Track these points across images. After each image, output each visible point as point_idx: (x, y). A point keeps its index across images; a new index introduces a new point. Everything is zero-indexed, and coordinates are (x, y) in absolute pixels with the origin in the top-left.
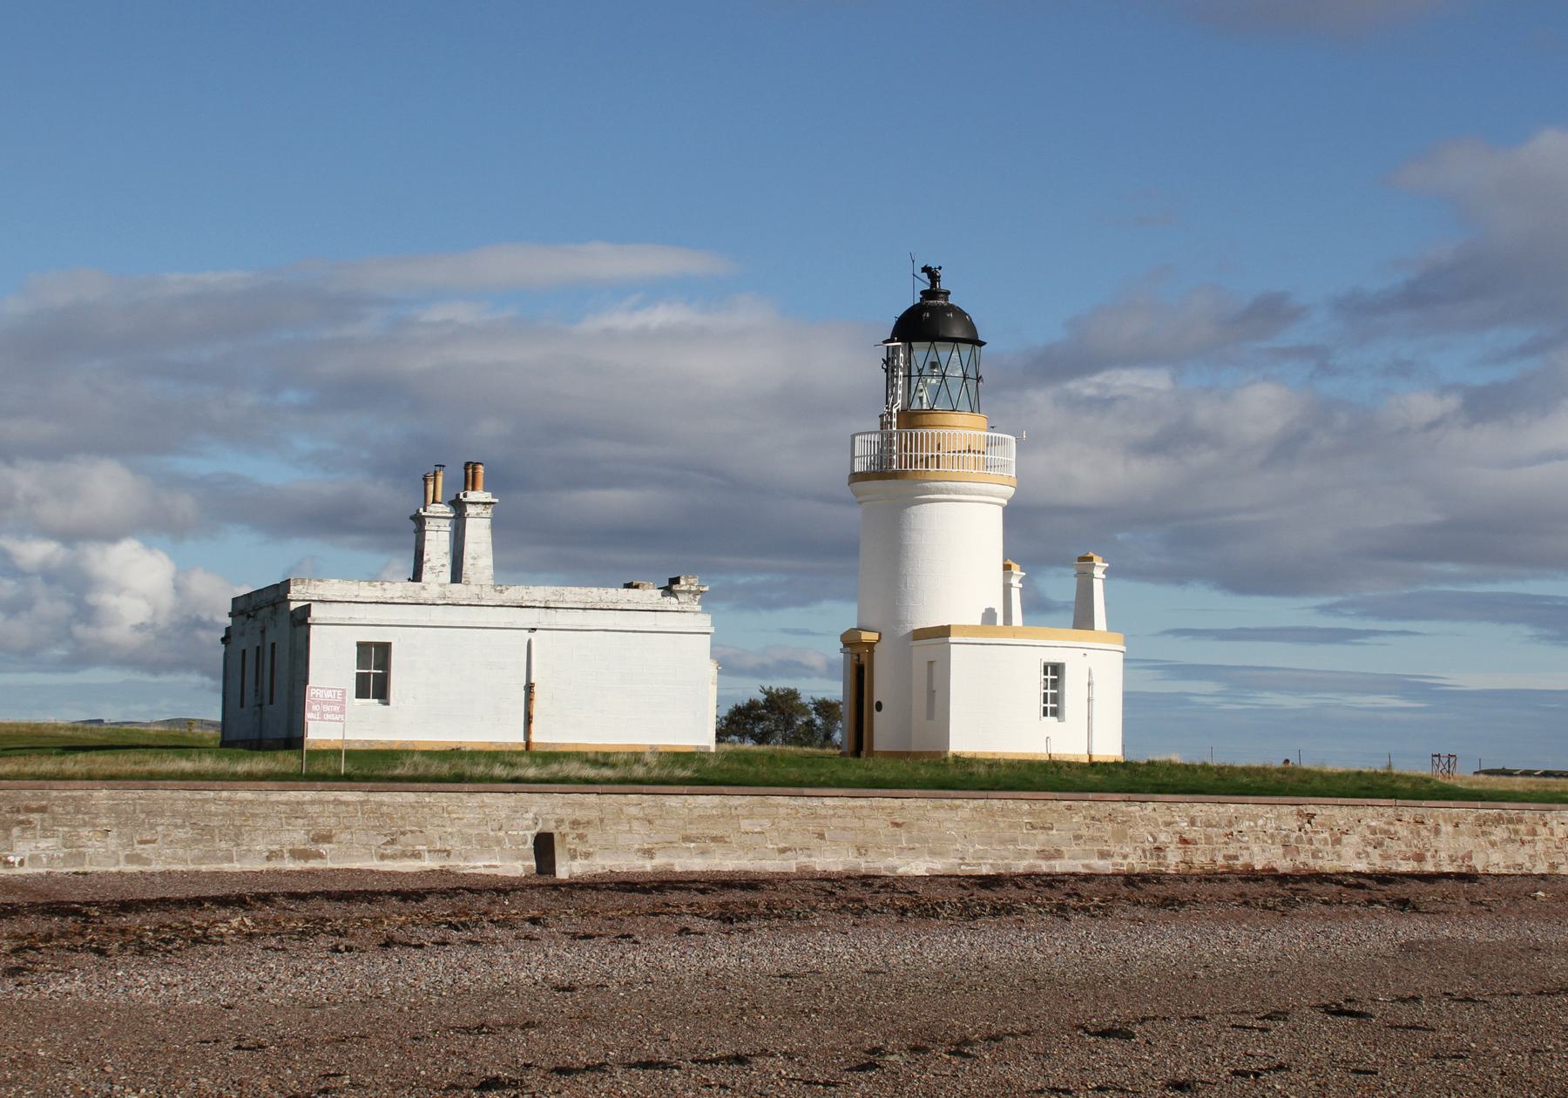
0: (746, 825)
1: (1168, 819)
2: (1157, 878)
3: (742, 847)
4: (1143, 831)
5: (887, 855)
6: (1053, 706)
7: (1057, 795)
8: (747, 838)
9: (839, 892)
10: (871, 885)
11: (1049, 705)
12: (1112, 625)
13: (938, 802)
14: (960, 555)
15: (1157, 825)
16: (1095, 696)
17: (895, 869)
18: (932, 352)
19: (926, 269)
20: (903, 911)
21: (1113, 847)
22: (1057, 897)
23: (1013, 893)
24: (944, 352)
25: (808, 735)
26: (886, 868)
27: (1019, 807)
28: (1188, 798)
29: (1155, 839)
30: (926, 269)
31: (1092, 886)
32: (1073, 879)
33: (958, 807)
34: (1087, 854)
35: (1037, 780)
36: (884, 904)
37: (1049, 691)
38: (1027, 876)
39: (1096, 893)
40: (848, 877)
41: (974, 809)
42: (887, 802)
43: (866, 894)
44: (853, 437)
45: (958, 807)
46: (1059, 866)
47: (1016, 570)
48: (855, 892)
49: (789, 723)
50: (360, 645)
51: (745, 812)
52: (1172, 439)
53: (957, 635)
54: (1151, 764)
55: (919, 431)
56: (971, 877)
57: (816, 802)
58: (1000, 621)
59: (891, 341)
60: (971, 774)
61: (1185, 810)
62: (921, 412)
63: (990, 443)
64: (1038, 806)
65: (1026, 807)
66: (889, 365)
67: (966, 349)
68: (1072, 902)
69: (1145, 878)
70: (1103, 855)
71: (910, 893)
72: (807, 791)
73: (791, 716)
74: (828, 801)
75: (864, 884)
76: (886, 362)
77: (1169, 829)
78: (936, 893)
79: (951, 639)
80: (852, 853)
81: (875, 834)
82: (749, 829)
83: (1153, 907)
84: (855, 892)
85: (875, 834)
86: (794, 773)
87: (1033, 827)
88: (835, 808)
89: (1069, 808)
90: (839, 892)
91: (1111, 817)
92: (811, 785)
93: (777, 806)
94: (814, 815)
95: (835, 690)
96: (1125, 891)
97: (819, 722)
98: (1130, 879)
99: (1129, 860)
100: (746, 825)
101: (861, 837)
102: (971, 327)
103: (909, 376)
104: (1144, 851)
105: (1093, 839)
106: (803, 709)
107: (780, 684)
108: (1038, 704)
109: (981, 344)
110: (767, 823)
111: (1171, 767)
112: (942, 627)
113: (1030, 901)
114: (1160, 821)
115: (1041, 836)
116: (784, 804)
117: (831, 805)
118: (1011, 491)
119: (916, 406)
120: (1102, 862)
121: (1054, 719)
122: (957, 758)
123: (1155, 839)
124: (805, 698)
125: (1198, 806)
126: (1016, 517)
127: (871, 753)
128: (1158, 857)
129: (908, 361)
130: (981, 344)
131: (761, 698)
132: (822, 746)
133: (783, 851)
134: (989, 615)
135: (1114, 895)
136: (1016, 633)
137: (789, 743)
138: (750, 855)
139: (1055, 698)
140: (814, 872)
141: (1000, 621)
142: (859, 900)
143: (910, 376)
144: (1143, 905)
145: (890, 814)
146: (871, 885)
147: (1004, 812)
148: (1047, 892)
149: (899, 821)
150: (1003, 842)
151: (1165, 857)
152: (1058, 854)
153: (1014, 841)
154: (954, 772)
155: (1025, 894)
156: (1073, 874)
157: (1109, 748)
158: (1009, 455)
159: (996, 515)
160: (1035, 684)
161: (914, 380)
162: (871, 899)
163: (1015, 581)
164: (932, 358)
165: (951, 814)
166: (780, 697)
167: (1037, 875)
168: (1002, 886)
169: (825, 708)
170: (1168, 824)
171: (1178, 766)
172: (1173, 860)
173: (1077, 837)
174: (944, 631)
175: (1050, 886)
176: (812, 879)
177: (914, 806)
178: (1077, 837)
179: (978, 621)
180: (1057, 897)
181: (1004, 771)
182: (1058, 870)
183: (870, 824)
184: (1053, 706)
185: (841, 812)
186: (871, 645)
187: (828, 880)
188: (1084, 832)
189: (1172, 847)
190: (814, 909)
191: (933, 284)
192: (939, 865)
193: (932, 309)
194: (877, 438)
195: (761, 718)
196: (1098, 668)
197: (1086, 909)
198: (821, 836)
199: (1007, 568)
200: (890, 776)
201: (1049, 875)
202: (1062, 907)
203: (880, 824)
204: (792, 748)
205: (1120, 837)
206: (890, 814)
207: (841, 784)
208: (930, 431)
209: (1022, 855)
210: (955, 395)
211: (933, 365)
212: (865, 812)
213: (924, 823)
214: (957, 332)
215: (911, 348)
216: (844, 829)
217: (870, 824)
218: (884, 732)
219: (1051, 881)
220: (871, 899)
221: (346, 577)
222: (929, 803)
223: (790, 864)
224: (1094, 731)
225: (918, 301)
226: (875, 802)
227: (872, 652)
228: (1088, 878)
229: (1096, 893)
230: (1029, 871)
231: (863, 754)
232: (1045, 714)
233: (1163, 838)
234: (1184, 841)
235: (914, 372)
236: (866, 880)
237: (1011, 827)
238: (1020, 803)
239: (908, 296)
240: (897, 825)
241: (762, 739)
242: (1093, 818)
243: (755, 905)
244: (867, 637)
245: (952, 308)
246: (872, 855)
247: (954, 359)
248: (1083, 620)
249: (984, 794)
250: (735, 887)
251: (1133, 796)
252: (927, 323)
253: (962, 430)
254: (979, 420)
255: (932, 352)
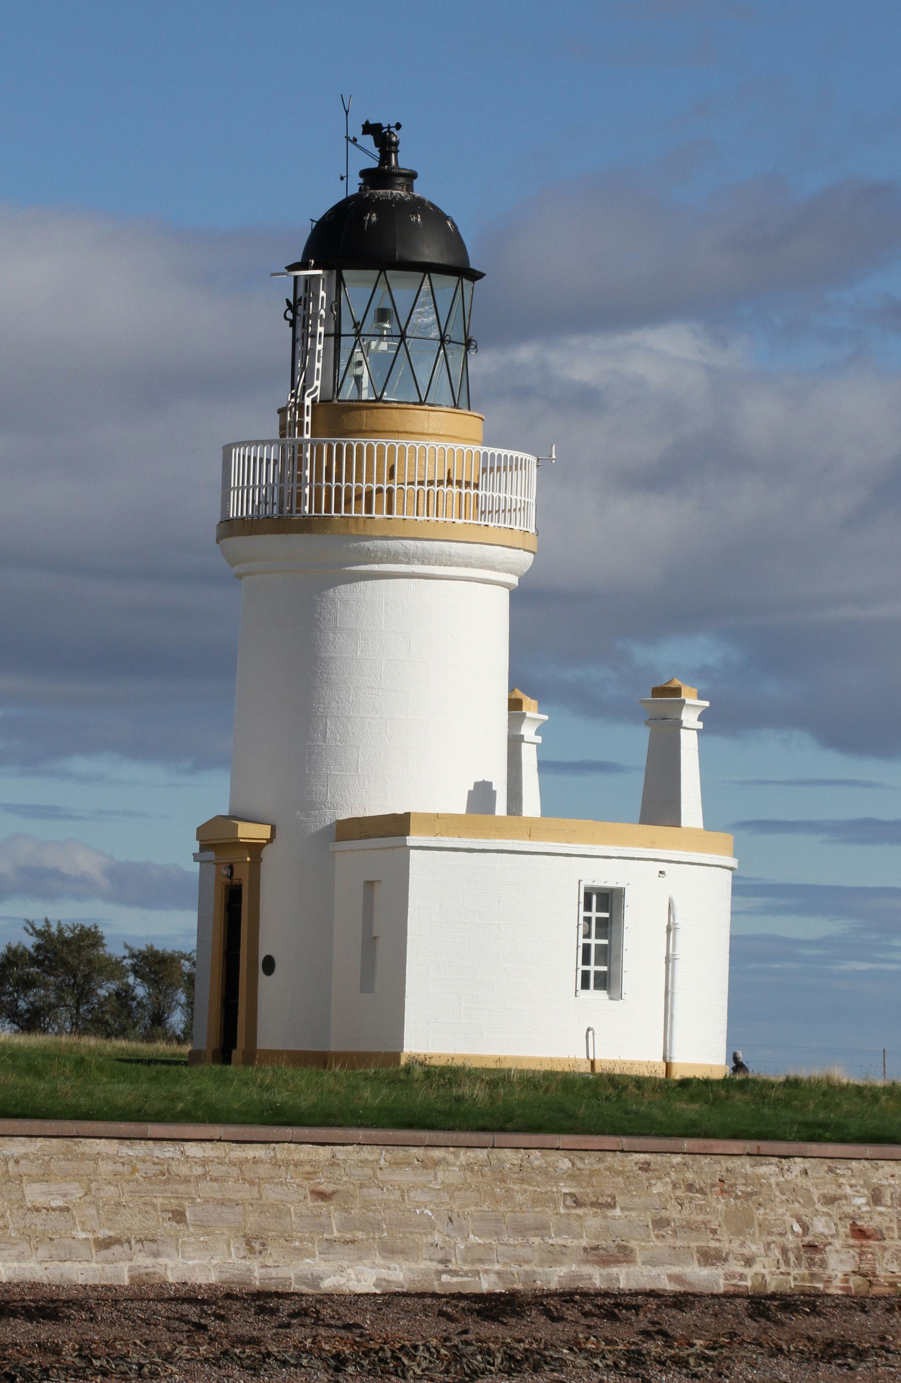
0: (34, 1193)
1: (831, 1190)
2: (807, 1303)
3: (27, 1235)
4: (782, 1213)
5: (300, 1253)
6: (601, 968)
7: (625, 1142)
8: (37, 1219)
9: (214, 1325)
10: (273, 1312)
11: (592, 968)
12: (711, 821)
13: (400, 1153)
14: (430, 682)
15: (809, 1202)
16: (681, 951)
17: (316, 1279)
18: (381, 289)
19: (369, 128)
20: (339, 1363)
21: (728, 1243)
22: (625, 1336)
23: (544, 1329)
24: (403, 288)
25: (119, 1016)
26: (301, 1279)
27: (554, 1164)
28: (869, 1150)
29: (806, 1228)
30: (369, 128)
31: (689, 1317)
32: (653, 1303)
33: (437, 1163)
34: (678, 1255)
35: (582, 1111)
36: (301, 1350)
37: (593, 941)
38: (568, 1296)
39: (698, 1331)
40: (229, 1296)
41: (468, 1167)
42: (304, 1152)
43: (265, 1329)
44: (227, 451)
45: (437, 1163)
46: (626, 1278)
47: (531, 709)
48: (244, 1324)
49: (83, 993)
50: (373, 992)
51: (34, 1169)
52: (692, 459)
53: (420, 833)
54: (792, 1084)
55: (355, 442)
56: (460, 1296)
57: (169, 1151)
58: (501, 808)
59: (304, 265)
60: (459, 1099)
61: (863, 1173)
62: (357, 405)
63: (489, 467)
64: (588, 1162)
65: (564, 1164)
66: (298, 310)
67: (445, 285)
68: (654, 1347)
69: (787, 1303)
70: (708, 1257)
71: (348, 1327)
72: (154, 1129)
73: (88, 978)
74: (193, 1149)
75: (261, 1310)
76: (292, 307)
77: (833, 1210)
78: (398, 1328)
79: (411, 840)
80: (237, 1248)
81: (280, 1212)
82: (41, 1201)
83: (806, 1358)
84: (244, 1324)
85: (280, 1212)
86: (123, 1092)
87: (578, 1203)
88: (204, 1162)
89: (645, 1167)
90: (214, 1325)
91: (724, 1186)
92: (159, 1118)
93: (96, 1158)
94: (166, 1176)
95: (178, 928)
96: (751, 1328)
97: (141, 991)
98: (762, 1304)
99: (757, 1268)
100: (34, 1193)
101: (253, 1219)
102: (455, 241)
103: (337, 336)
104: (784, 1251)
105: (690, 1227)
106: (113, 968)
107: (66, 914)
108: (569, 965)
109: (475, 276)
110: (75, 1191)
111: (830, 1091)
112: (394, 816)
113: (575, 1346)
114: (816, 1194)
115: (593, 1221)
116: (107, 1153)
117: (197, 1155)
118: (526, 559)
119: (348, 392)
120: (705, 1272)
121: (602, 994)
122: (417, 1062)
123: (806, 1228)
124: (114, 949)
125: (888, 1168)
126: (529, 602)
127: (250, 1057)
128: (811, 1263)
129: (336, 306)
130: (475, 276)
131: (30, 942)
132: (149, 1038)
133: (105, 1244)
134: (481, 795)
135: (732, 1335)
136: (531, 830)
137: (84, 1032)
138: (42, 1252)
139: (607, 955)
140: (164, 1285)
141: (501, 808)
142: (254, 1341)
143: (338, 336)
144: (788, 1356)
145: (309, 1176)
146: (273, 1312)
147: (523, 1173)
148: (606, 1328)
149: (326, 1187)
150: (520, 1230)
151: (823, 1264)
152: (624, 1255)
153: (541, 1229)
154: (423, 1096)
155: (564, 1331)
156: (652, 1294)
157: (703, 1053)
158: (527, 494)
159: (502, 597)
160: (564, 931)
161: (347, 343)
162: (275, 1338)
163: (528, 731)
164: (381, 300)
165: (422, 1177)
166: (66, 942)
167: (585, 1294)
168: (519, 1315)
169: (155, 966)
170: (829, 1200)
171: (844, 1089)
172: (839, 1269)
173: (660, 1223)
174: (397, 825)
175: (611, 1316)
176: (160, 1300)
177: (357, 1161)
178: (660, 1223)
179: (460, 807)
180: (625, 1336)
181: (518, 1095)
182: (623, 1284)
183: (271, 1194)
184: (601, 968)
185: (215, 1170)
186: (255, 849)
187: (191, 1301)
188: (673, 1212)
189: (838, 1243)
190: (168, 1357)
191: (385, 158)
192: (400, 1274)
193: (382, 206)
194: (273, 453)
195: (27, 984)
196: (685, 898)
197: (680, 1362)
198: (179, 1216)
199: (515, 705)
200: (306, 1101)
201: (606, 1294)
202: (635, 1358)
203: (290, 1194)
204: (92, 1042)
205: (741, 1224)
206: (309, 1176)
207: (215, 1116)
208: (365, 442)
209: (555, 1256)
210: (423, 379)
211: (383, 315)
212: (262, 1171)
213: (373, 1193)
214: (429, 253)
215: (340, 281)
216: (222, 1203)
217: (271, 1194)
218: (278, 1015)
219: (613, 1306)
220: (275, 1338)
221: (448, 834)
222: (382, 1156)
223: (118, 1270)
224: (674, 1020)
225: (354, 190)
226: (282, 1151)
227: (257, 861)
228: (682, 1301)
229: (698, 1331)
230: (568, 1286)
231: (236, 1054)
232: (585, 985)
233: (820, 1226)
234: (860, 1233)
235: (347, 328)
236: (264, 1301)
237: (535, 1201)
238: (553, 1156)
239: (330, 180)
240: (322, 1196)
241: (30, 1022)
242: (690, 1187)
243: (56, 1351)
244: (247, 832)
245: (419, 205)
246: (274, 1254)
247: (422, 305)
248: (660, 807)
249: (486, 1137)
250: (14, 1314)
251: (766, 1146)
252: (368, 232)
253: (436, 441)
254: (467, 423)
255: (381, 289)
